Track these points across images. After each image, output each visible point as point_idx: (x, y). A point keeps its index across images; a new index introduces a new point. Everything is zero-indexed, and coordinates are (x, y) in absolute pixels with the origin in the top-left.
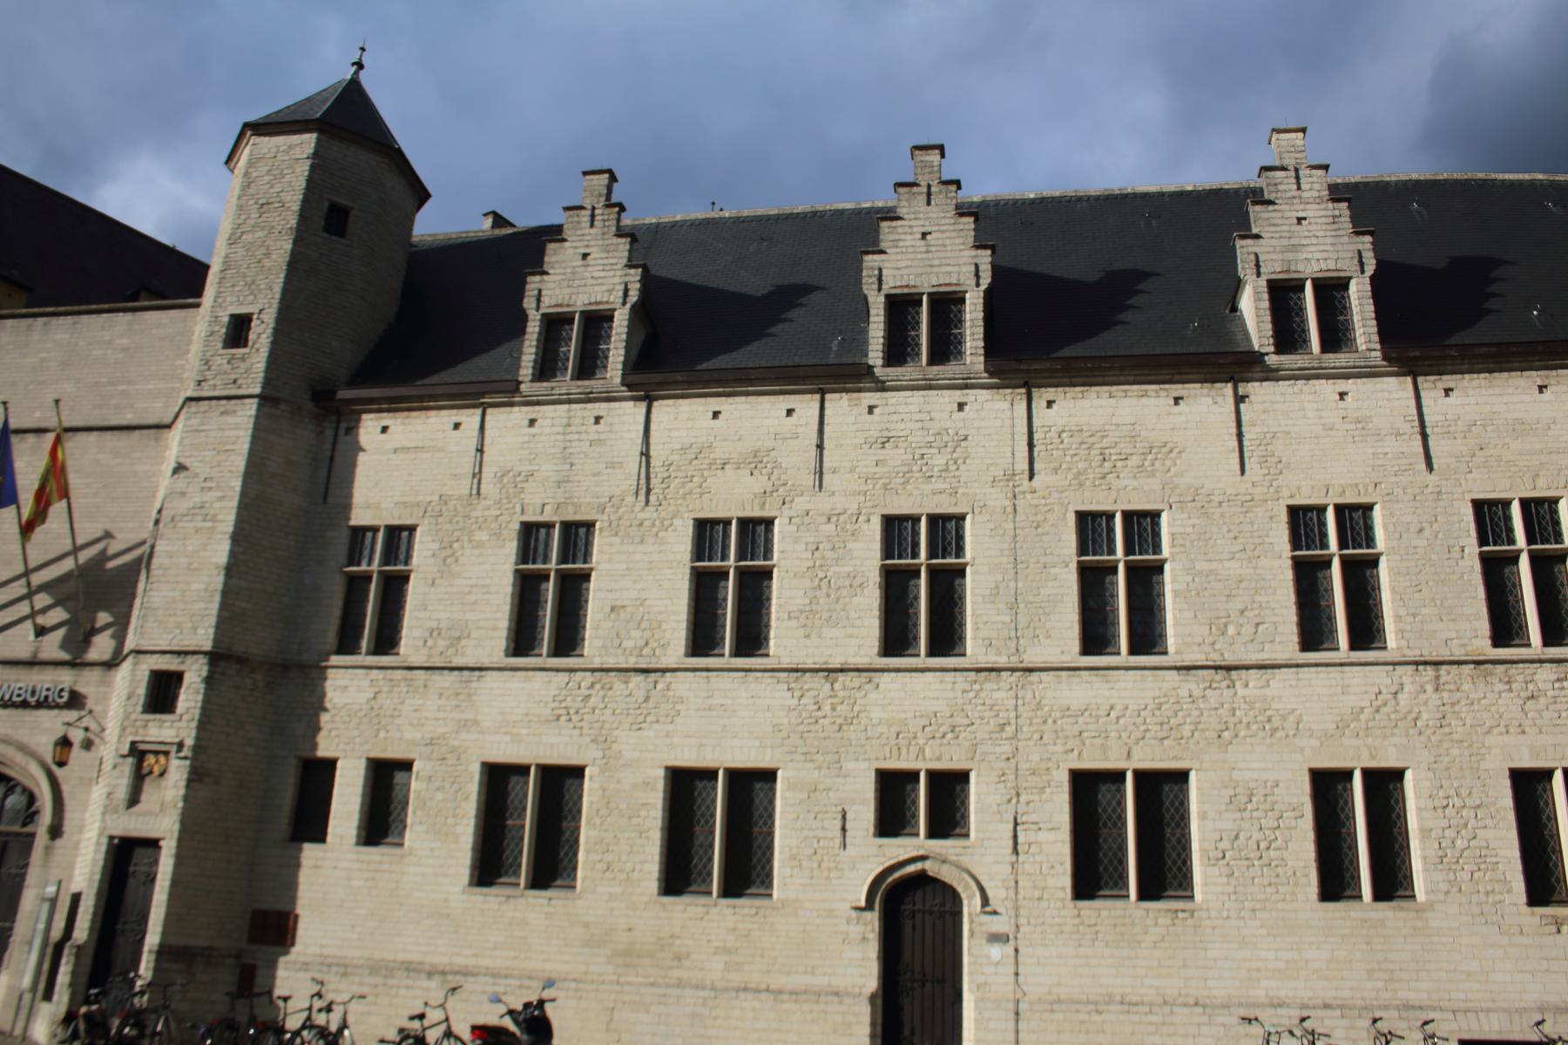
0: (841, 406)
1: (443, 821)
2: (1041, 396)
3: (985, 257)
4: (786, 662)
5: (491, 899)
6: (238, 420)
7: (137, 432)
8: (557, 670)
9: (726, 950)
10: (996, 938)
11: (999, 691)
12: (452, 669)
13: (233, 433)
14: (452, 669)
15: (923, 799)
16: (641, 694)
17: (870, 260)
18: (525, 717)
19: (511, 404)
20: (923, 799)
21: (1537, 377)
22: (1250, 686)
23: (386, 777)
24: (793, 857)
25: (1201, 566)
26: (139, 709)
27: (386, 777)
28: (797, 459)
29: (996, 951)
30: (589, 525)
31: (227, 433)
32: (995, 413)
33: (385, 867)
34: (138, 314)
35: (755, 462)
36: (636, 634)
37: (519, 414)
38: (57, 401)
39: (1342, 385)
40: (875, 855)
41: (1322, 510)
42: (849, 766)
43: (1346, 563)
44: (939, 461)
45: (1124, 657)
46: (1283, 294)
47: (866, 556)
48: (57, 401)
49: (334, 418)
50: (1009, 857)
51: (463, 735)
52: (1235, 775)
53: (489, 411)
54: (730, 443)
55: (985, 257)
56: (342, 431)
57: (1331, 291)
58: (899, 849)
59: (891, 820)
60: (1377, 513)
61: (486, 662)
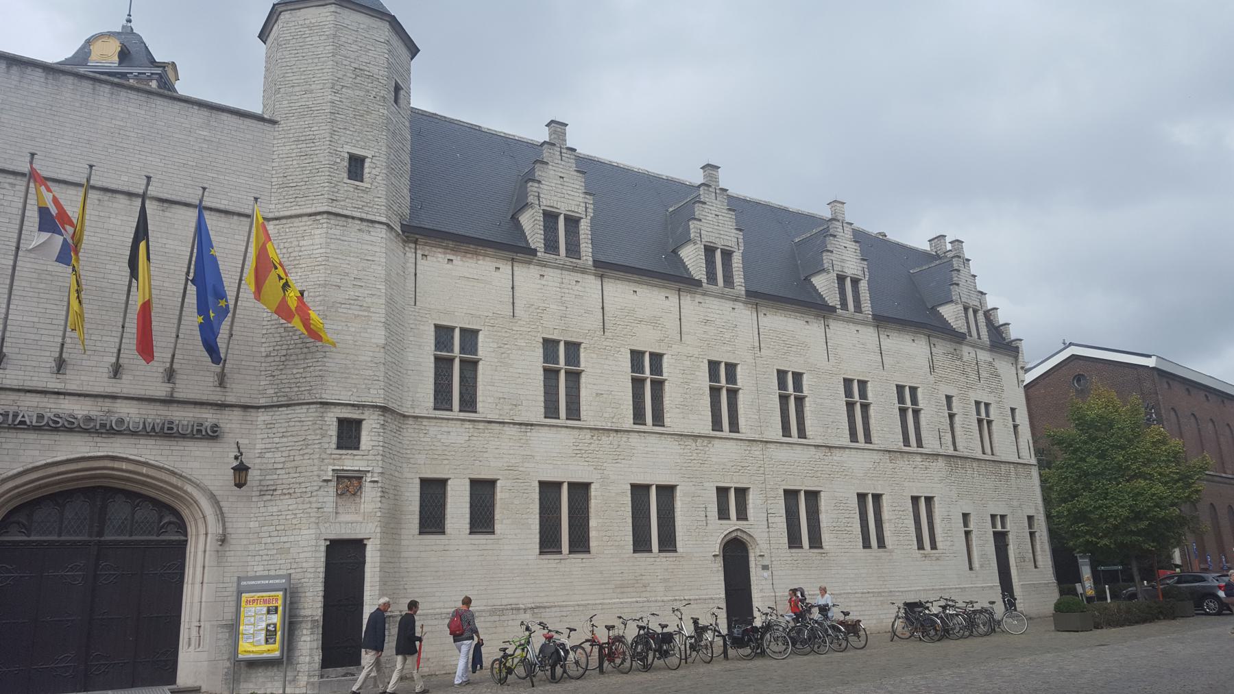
0: (687, 300)
1: (518, 516)
2: (762, 310)
3: (590, 199)
4: (677, 430)
5: (550, 561)
6: (373, 239)
7: (236, 217)
8: (573, 428)
9: (665, 580)
10: (765, 568)
11: (757, 450)
12: (515, 424)
13: (370, 248)
14: (515, 424)
15: (732, 500)
16: (615, 443)
17: (692, 224)
18: (557, 454)
19: (530, 263)
20: (732, 500)
21: (633, 287)
22: (837, 456)
23: (483, 490)
24: (688, 530)
25: (818, 401)
26: (334, 446)
27: (483, 490)
28: (671, 323)
29: (766, 574)
30: (579, 344)
31: (365, 247)
32: (744, 315)
33: (488, 547)
34: (215, 114)
35: (654, 322)
36: (610, 410)
37: (534, 271)
38: (33, 155)
39: (859, 327)
41: (643, 353)
42: (706, 484)
43: (652, 381)
44: (727, 336)
45: (456, 413)
46: (550, 218)
47: (703, 380)
48: (33, 155)
49: (413, 245)
51: (526, 465)
53: (141, 192)
54: (644, 313)
55: (740, 235)
56: (419, 256)
57: (573, 222)
59: (723, 514)
60: (869, 384)
61: (533, 420)
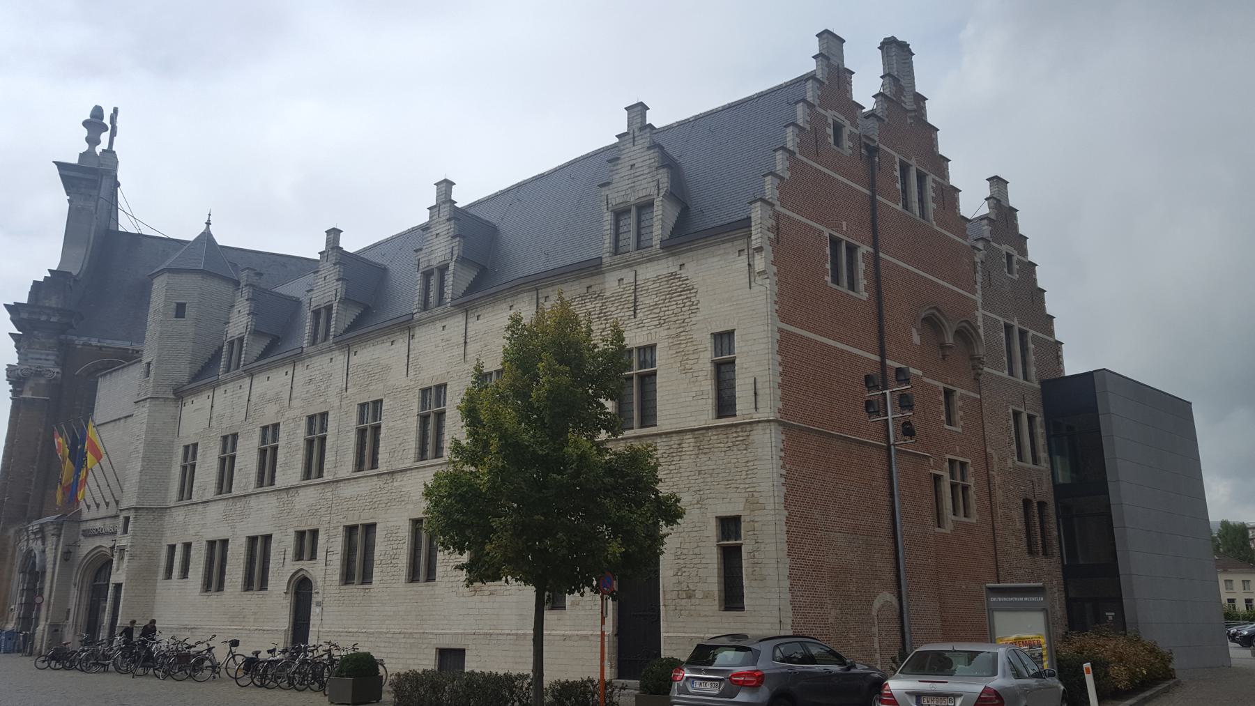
11: (328, 490)
15: (306, 543)
40: (291, 567)
50: (325, 570)
52: (389, 524)
58: (299, 565)
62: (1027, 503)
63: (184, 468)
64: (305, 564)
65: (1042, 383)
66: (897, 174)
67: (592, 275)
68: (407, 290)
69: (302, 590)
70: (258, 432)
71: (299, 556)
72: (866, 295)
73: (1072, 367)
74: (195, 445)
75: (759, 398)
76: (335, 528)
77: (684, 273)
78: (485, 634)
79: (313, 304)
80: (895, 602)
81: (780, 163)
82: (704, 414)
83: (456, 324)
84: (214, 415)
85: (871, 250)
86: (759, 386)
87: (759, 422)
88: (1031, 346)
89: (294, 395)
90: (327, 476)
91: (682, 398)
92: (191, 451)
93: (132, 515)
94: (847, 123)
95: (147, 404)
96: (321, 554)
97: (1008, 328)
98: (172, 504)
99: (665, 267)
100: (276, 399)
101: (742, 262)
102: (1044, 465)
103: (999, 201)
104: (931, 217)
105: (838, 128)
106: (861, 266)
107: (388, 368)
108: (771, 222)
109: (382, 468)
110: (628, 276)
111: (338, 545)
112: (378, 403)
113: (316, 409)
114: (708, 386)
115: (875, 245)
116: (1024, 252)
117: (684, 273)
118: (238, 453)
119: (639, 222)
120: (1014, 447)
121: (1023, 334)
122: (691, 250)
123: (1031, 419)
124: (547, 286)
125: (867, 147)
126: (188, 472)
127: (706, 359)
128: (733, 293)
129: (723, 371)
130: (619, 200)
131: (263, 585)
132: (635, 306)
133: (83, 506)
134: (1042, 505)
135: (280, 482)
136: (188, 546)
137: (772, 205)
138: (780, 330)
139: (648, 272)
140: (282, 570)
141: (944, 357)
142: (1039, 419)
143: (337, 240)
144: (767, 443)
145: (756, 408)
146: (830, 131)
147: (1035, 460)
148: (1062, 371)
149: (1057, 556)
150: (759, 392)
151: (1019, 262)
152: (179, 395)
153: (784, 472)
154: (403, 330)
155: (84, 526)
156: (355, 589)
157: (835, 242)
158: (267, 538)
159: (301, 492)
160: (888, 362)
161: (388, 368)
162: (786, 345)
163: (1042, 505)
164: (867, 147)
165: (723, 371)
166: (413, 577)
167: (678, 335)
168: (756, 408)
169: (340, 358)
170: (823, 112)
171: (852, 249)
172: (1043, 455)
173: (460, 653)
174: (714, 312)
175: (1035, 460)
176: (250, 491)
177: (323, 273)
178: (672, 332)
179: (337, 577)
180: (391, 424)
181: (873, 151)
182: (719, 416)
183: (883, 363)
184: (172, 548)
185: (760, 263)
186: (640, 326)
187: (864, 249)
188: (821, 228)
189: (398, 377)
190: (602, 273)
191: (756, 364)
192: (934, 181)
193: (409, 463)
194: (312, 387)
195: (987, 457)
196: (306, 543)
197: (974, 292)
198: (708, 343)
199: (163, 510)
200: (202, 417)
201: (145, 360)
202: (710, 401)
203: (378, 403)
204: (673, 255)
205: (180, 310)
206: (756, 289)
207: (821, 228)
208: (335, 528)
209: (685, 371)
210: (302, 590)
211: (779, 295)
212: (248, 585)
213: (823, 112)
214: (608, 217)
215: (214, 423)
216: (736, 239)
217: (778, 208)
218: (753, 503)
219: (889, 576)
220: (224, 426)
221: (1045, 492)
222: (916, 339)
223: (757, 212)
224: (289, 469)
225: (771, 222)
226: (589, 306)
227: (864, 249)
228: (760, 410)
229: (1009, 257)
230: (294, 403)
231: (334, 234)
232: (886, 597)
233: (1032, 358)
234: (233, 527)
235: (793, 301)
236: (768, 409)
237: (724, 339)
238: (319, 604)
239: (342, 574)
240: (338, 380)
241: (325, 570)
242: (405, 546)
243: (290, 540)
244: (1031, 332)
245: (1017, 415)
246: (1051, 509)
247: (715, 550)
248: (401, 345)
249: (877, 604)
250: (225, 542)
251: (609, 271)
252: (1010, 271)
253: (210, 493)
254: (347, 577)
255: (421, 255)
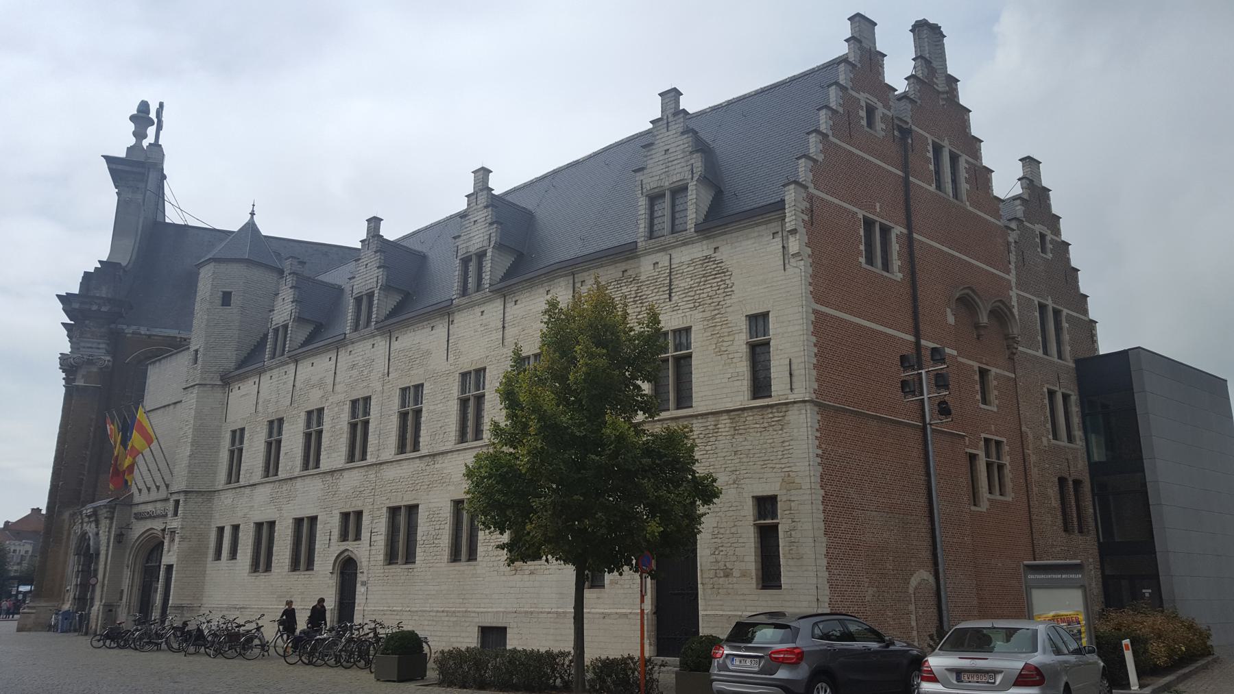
15: (351, 524)
40: (337, 547)
62: (1062, 481)
63: (232, 452)
64: (350, 545)
65: (1077, 361)
66: (930, 155)
67: (628, 259)
68: (446, 275)
69: (347, 569)
70: (303, 416)
71: (344, 537)
72: (900, 275)
73: (1106, 345)
74: (242, 430)
75: (794, 379)
76: (378, 509)
77: (718, 256)
78: (526, 612)
79: (355, 292)
80: (931, 579)
81: (814, 145)
82: (740, 395)
83: (494, 310)
84: (260, 401)
85: (905, 231)
86: (794, 367)
87: (795, 402)
88: (1065, 325)
89: (338, 380)
90: (370, 459)
91: (717, 379)
92: (238, 436)
93: (182, 498)
94: (879, 105)
95: (196, 390)
96: (365, 534)
97: (1042, 307)
98: (220, 487)
99: (699, 250)
100: (321, 384)
101: (776, 244)
102: (1080, 444)
103: (1031, 181)
104: (965, 197)
105: (871, 111)
106: (895, 247)
107: (429, 352)
108: (806, 205)
109: (424, 451)
110: (663, 260)
111: (382, 526)
112: (419, 388)
113: (359, 394)
114: (743, 367)
115: (909, 226)
116: (1057, 232)
117: (718, 256)
118: (284, 437)
119: (673, 206)
120: (1049, 426)
121: (1057, 313)
122: (725, 233)
123: (1066, 397)
124: (584, 271)
125: (900, 129)
126: (236, 456)
127: (740, 342)
128: (768, 276)
129: (759, 352)
130: (653, 185)
131: (310, 565)
132: (670, 289)
133: (134, 490)
134: (1077, 483)
135: (325, 464)
136: (236, 528)
137: (805, 187)
138: (815, 312)
139: (683, 256)
140: (327, 550)
141: (978, 337)
142: (1074, 398)
143: (377, 228)
144: (802, 427)
145: (792, 389)
146: (863, 114)
147: (1070, 438)
148: (1097, 350)
149: (1093, 533)
150: (795, 373)
151: (1052, 241)
152: (227, 381)
153: (820, 452)
154: (442, 315)
155: (135, 510)
156: (399, 569)
157: (869, 224)
158: (313, 520)
159: (346, 474)
160: (923, 342)
161: (429, 352)
162: (820, 325)
163: (1077, 483)
164: (900, 129)
165: (759, 352)
166: (455, 557)
167: (713, 317)
168: (792, 389)
169: (381, 344)
170: (854, 94)
171: (885, 231)
172: (1078, 433)
173: (502, 631)
174: (749, 294)
175: (1070, 438)
176: (296, 474)
177: (364, 261)
178: (707, 314)
179: (381, 557)
180: (432, 408)
181: (905, 132)
182: (755, 397)
183: (918, 344)
184: (221, 530)
185: (794, 245)
186: (676, 308)
187: (898, 230)
188: (855, 209)
189: (438, 361)
190: (637, 257)
191: (791, 345)
192: (967, 162)
193: (450, 445)
194: (355, 372)
195: (1022, 435)
196: (351, 524)
197: (1008, 272)
198: (743, 325)
199: (210, 494)
200: (249, 402)
201: (193, 348)
202: (745, 383)
203: (419, 388)
204: (708, 238)
205: (226, 299)
206: (790, 270)
207: (855, 209)
208: (378, 509)
209: (720, 353)
210: (347, 569)
211: (814, 276)
212: (295, 566)
213: (854, 94)
214: (643, 202)
215: (260, 408)
216: (769, 221)
217: (812, 190)
218: (789, 482)
219: (926, 554)
220: (270, 410)
221: (1080, 469)
222: (951, 319)
223: (791, 195)
224: (334, 453)
225: (806, 205)
226: (625, 290)
227: (898, 230)
228: (795, 391)
229: (1043, 236)
230: (338, 388)
231: (374, 222)
232: (923, 576)
233: (1066, 337)
234: (280, 510)
235: (827, 283)
236: (803, 391)
237: (758, 321)
238: (364, 584)
239: (386, 554)
240: (381, 365)
241: (369, 550)
242: (447, 526)
243: (335, 522)
244: (1065, 311)
245: (1051, 394)
246: (1087, 487)
247: (752, 529)
248: (441, 330)
249: (914, 582)
250: (272, 524)
251: (644, 255)
252: (1044, 250)
253: (257, 476)
254: (391, 558)
255: (459, 242)
